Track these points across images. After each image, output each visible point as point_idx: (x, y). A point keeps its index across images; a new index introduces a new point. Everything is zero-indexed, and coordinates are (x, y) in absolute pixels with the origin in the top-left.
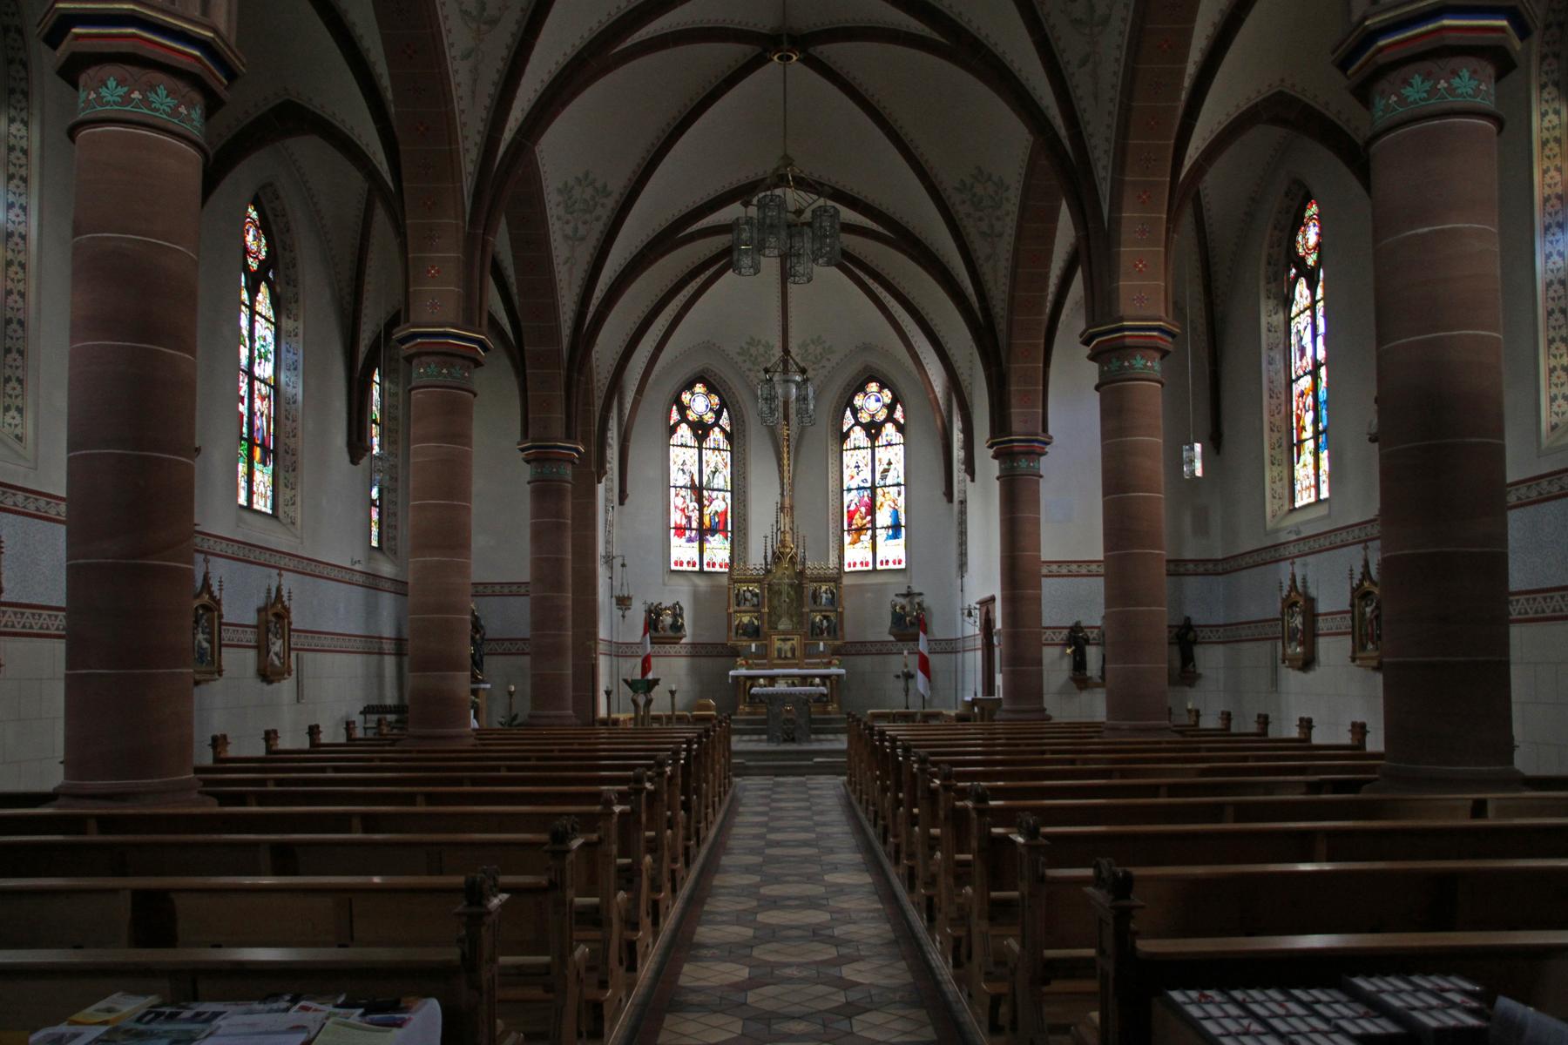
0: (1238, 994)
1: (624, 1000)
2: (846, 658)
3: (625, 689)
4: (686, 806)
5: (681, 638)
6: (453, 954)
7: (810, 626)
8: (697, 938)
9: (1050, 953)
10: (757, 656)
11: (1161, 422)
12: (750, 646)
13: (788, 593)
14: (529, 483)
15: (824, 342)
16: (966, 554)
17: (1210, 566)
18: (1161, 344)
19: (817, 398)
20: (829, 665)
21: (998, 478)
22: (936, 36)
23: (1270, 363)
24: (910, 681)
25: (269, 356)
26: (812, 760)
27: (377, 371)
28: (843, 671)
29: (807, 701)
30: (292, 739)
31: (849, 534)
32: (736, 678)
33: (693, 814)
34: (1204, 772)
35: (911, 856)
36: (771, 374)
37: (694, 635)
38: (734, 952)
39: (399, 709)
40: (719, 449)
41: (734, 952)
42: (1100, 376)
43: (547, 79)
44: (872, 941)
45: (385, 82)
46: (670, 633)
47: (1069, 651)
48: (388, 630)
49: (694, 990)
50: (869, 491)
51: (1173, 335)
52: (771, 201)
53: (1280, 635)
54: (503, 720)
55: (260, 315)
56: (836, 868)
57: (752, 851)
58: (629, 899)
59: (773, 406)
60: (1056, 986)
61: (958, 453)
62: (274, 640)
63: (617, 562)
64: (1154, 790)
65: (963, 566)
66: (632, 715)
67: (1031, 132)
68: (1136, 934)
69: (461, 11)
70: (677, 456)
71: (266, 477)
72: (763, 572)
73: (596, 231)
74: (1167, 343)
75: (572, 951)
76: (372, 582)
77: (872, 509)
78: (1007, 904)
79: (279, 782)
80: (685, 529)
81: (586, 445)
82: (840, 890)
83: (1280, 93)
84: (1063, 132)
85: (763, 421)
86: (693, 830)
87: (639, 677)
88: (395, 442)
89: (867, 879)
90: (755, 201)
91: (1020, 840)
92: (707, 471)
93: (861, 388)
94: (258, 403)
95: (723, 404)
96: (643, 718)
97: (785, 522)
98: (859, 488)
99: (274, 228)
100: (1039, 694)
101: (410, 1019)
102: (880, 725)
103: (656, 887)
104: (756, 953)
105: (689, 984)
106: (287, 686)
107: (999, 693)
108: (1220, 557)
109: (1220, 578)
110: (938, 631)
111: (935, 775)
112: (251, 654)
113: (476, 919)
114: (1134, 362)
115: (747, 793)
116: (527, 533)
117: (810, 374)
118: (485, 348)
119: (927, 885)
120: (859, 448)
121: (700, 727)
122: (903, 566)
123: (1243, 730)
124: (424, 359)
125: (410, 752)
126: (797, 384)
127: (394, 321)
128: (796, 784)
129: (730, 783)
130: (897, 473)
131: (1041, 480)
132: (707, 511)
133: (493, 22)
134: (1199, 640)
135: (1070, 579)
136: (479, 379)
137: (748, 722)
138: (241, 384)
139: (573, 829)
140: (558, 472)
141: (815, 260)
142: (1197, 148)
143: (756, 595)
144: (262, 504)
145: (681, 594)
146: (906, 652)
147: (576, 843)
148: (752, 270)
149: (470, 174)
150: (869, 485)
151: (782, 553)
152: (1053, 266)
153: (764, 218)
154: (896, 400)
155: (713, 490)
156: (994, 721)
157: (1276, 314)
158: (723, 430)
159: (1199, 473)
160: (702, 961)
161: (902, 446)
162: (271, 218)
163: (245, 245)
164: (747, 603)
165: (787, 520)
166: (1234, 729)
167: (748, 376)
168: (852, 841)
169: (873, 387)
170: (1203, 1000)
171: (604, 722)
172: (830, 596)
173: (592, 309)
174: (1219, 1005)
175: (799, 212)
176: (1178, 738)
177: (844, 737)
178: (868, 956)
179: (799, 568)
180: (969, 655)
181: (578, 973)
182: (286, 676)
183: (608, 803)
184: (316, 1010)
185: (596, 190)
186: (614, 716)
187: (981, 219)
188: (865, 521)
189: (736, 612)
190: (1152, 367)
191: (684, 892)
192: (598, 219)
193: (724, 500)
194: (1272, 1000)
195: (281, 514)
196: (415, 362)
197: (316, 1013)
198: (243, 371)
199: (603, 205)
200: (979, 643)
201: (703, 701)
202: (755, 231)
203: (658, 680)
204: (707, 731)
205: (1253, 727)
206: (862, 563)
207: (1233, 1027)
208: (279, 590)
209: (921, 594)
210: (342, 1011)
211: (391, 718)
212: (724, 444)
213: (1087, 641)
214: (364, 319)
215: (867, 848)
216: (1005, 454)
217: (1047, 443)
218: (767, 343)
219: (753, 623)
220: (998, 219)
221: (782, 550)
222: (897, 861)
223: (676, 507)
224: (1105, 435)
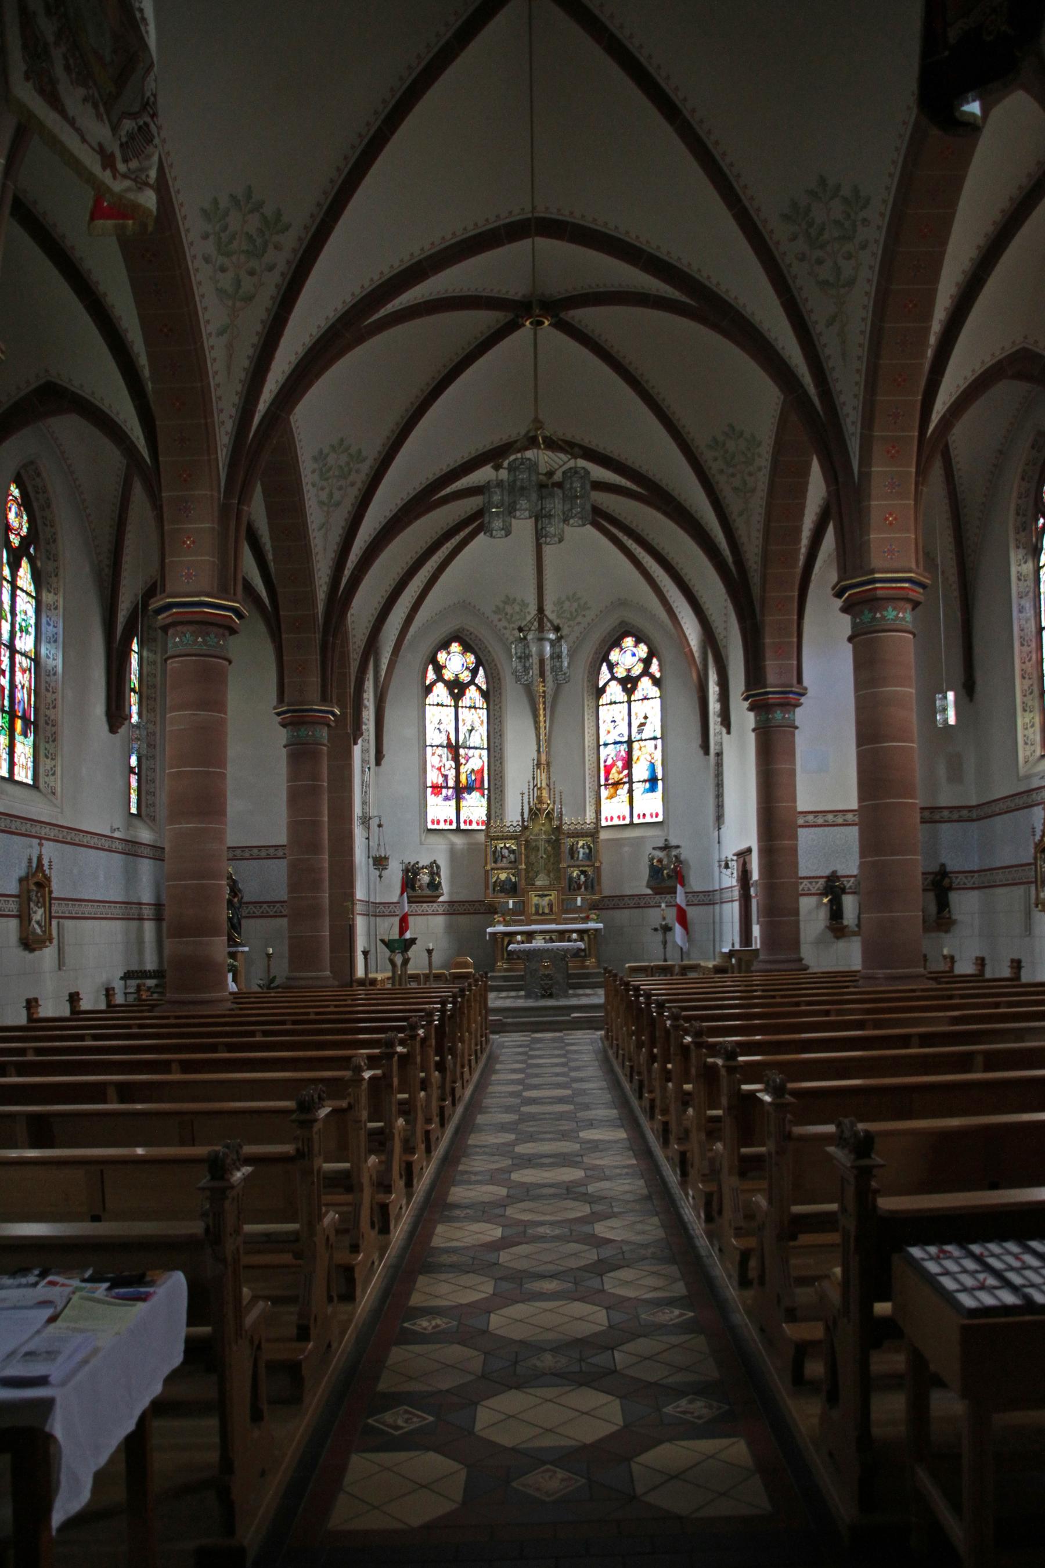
0: (976, 1248)
1: (376, 1263)
2: (605, 912)
3: (382, 948)
4: (441, 1067)
5: (438, 897)
6: (196, 1228)
7: (567, 881)
8: (451, 1199)
9: (796, 1209)
10: (514, 912)
11: (913, 672)
12: (508, 902)
13: (545, 849)
14: (285, 747)
15: (579, 598)
16: (722, 806)
17: (964, 813)
18: (912, 595)
19: (572, 655)
20: (586, 919)
21: (754, 730)
22: (684, 299)
23: (1020, 612)
24: (669, 935)
25: (30, 629)
26: (569, 1015)
27: (135, 641)
28: (601, 926)
29: (565, 956)
30: (53, 1008)
31: (606, 789)
32: (494, 934)
33: (448, 1073)
34: (955, 1021)
35: (665, 1111)
36: (526, 633)
37: (451, 894)
38: (485, 1211)
39: (158, 974)
40: (475, 708)
41: (485, 1211)
42: (853, 628)
43: (301, 351)
44: (628, 1197)
45: (143, 361)
46: (427, 892)
47: (825, 900)
48: (147, 896)
49: (447, 1251)
50: (625, 745)
51: (923, 586)
52: (522, 463)
53: (1034, 880)
54: (261, 982)
55: (22, 590)
56: (592, 1125)
57: (508, 1109)
58: (380, 1162)
59: (527, 665)
60: (804, 1239)
61: (714, 706)
62: (35, 908)
63: (373, 823)
64: (905, 1041)
65: (719, 818)
66: (390, 974)
67: (781, 390)
68: (876, 1192)
69: (217, 289)
70: (433, 715)
71: (27, 748)
72: (519, 829)
73: (353, 495)
74: (918, 594)
75: (320, 1217)
76: (131, 849)
77: (628, 764)
78: (757, 1160)
79: (39, 1051)
80: (442, 787)
81: (342, 708)
82: (595, 1146)
83: (1024, 350)
84: (812, 390)
85: (518, 679)
86: (448, 1089)
87: (397, 937)
88: (154, 710)
89: (622, 1135)
90: (506, 464)
91: (767, 1098)
92: (463, 730)
93: (617, 643)
94: (19, 676)
95: (479, 663)
96: (400, 977)
97: (542, 779)
98: (615, 743)
99: (35, 505)
100: (796, 944)
101: (154, 1292)
102: (636, 981)
103: (409, 1148)
104: (509, 1211)
105: (442, 1245)
106: (49, 953)
107: (757, 944)
108: (974, 803)
109: (975, 824)
110: (696, 883)
111: (687, 1032)
112: (13, 924)
113: (219, 1193)
114: (885, 613)
115: (503, 1051)
116: (284, 796)
117: (565, 631)
118: (240, 616)
119: (680, 1140)
120: (615, 703)
121: (455, 988)
122: (660, 819)
123: (997, 976)
124: (179, 628)
125: (168, 1018)
126: (552, 642)
127: (151, 592)
128: (553, 1040)
129: (487, 1041)
130: (654, 727)
131: (797, 731)
132: (463, 769)
133: (249, 299)
134: (954, 886)
135: (826, 829)
136: (234, 646)
137: (505, 978)
138: (3, 658)
139: (320, 1098)
140: (314, 735)
141: (566, 521)
142: (944, 403)
143: (513, 852)
144: (23, 775)
145: (437, 853)
146: (663, 905)
147: (323, 1112)
148: (503, 532)
149: (224, 445)
150: (625, 739)
151: (539, 810)
152: (807, 512)
153: (514, 481)
154: (651, 654)
155: (470, 748)
156: (752, 972)
157: (1025, 562)
158: (479, 688)
159: (952, 720)
160: (454, 1222)
161: (658, 700)
162: (32, 495)
163: (8, 522)
164: (505, 860)
165: (544, 776)
166: (988, 975)
167: (504, 634)
168: (608, 1097)
169: (629, 642)
170: (942, 1255)
171: (362, 982)
172: (587, 851)
173: (347, 573)
174: (956, 1260)
175: (550, 474)
176: (933, 985)
177: (601, 992)
178: (620, 1213)
179: (555, 823)
180: (726, 907)
181: (328, 1239)
182: (48, 944)
183: (358, 1070)
184: (63, 1285)
185: (350, 455)
186: (371, 976)
187: (733, 475)
188: (621, 776)
189: (493, 869)
190: (903, 619)
191: (439, 1152)
192: (353, 484)
193: (481, 758)
194: (1010, 1253)
195: (42, 785)
196: (171, 632)
197: (62, 1289)
198: (5, 645)
199: (358, 471)
200: (736, 894)
201: (461, 959)
202: (506, 493)
203: (416, 939)
204: (462, 990)
205: (1006, 973)
206: (619, 817)
207: (969, 1281)
208: (40, 859)
209: (678, 847)
210: (89, 1285)
211: (151, 982)
212: (480, 702)
213: (843, 891)
214: (122, 590)
215: (623, 1103)
216: (759, 706)
217: (803, 695)
218: (523, 601)
219: (510, 880)
220: (750, 474)
221: (539, 806)
222: (652, 1117)
223: (433, 766)
224: (858, 685)
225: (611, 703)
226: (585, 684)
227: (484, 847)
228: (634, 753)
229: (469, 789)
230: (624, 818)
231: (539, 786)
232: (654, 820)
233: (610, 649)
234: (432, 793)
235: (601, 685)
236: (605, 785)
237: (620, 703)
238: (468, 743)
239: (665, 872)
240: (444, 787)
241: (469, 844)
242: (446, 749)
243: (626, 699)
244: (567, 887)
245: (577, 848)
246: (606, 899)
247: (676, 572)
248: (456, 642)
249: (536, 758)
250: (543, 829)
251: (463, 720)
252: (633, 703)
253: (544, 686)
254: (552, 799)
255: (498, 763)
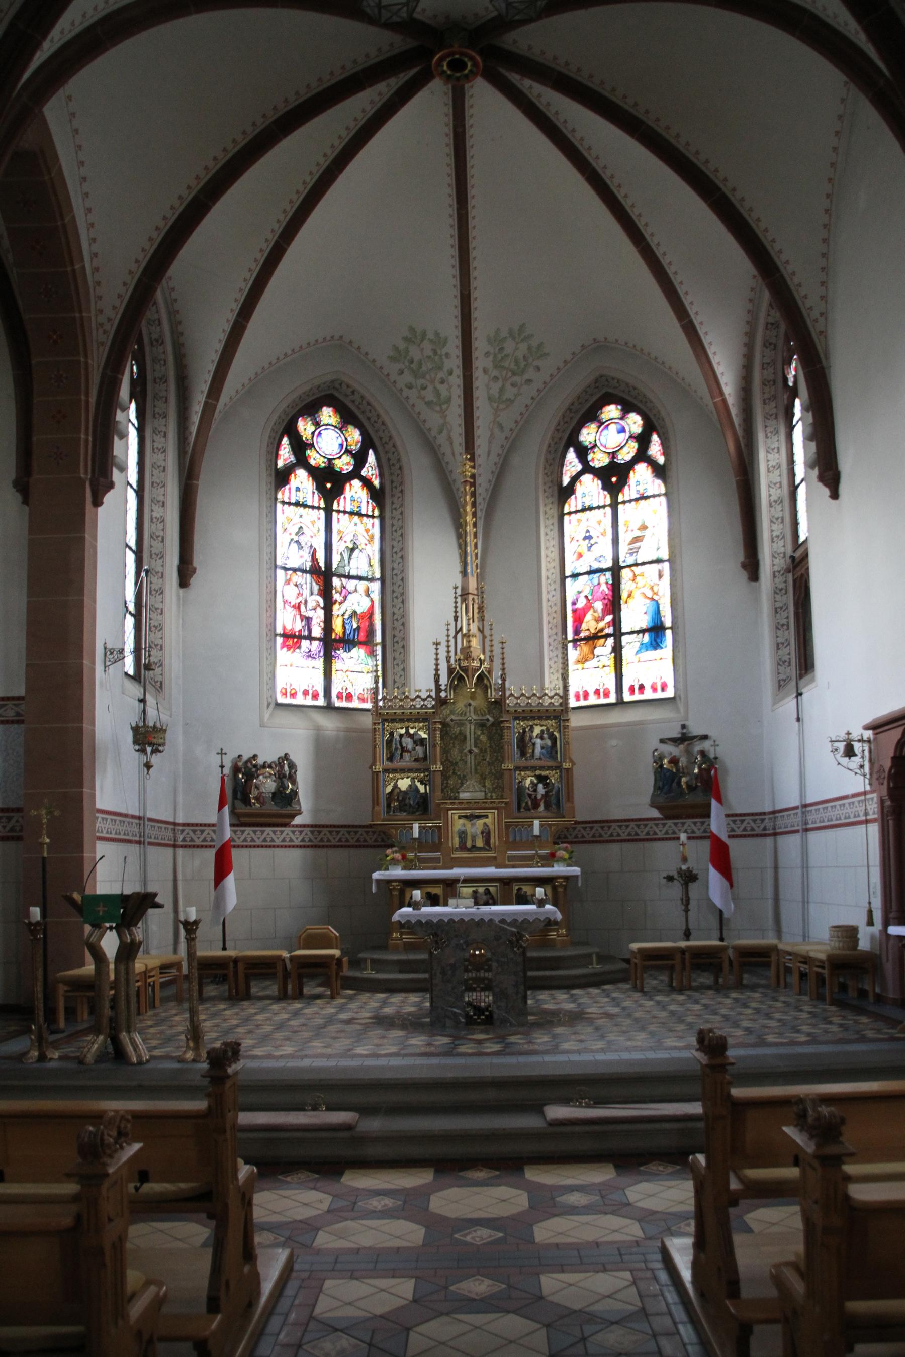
5: (293, 816)
10: (421, 845)
13: (477, 739)
15: (530, 336)
20: (551, 859)
24: (694, 888)
26: (538, 1108)
28: (576, 870)
29: (519, 936)
31: (575, 647)
37: (316, 811)
40: (359, 514)
46: (271, 807)
50: (608, 575)
72: (431, 703)
77: (614, 604)
80: (300, 637)
92: (338, 547)
93: (591, 415)
95: (367, 443)
120: (590, 508)
122: (670, 693)
143: (422, 742)
146: (683, 837)
150: (609, 564)
151: (465, 670)
155: (349, 577)
158: (367, 483)
161: (663, 499)
164: (407, 756)
172: (549, 743)
179: (493, 695)
188: (602, 624)
189: (386, 771)
193: (368, 595)
209: (705, 737)
212: (365, 503)
218: (437, 334)
221: (464, 664)
223: (285, 602)
225: (584, 510)
226: (541, 481)
227: (370, 735)
228: (623, 586)
229: (348, 643)
230: (607, 695)
231: (464, 631)
232: (660, 695)
233: (581, 425)
234: (284, 645)
235: (566, 481)
236: (575, 641)
237: (599, 507)
238: (347, 569)
239: (684, 779)
240: (305, 638)
241: (348, 730)
242: (308, 576)
243: (608, 501)
244: (515, 805)
245: (531, 738)
246: (579, 827)
247: (724, 197)
248: (329, 406)
249: (459, 585)
250: (473, 703)
251: (339, 532)
252: (620, 507)
253: (474, 467)
254: (488, 654)
255: (398, 602)
